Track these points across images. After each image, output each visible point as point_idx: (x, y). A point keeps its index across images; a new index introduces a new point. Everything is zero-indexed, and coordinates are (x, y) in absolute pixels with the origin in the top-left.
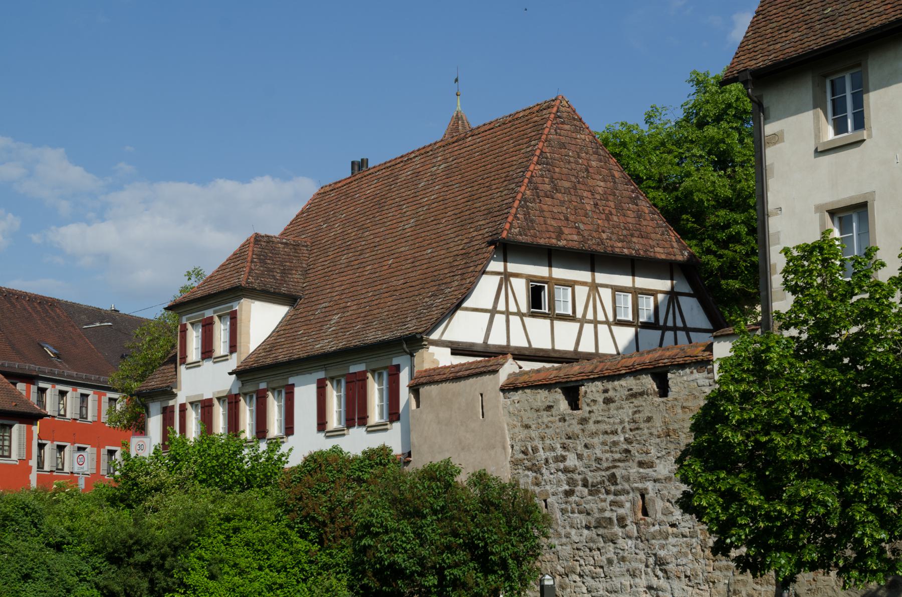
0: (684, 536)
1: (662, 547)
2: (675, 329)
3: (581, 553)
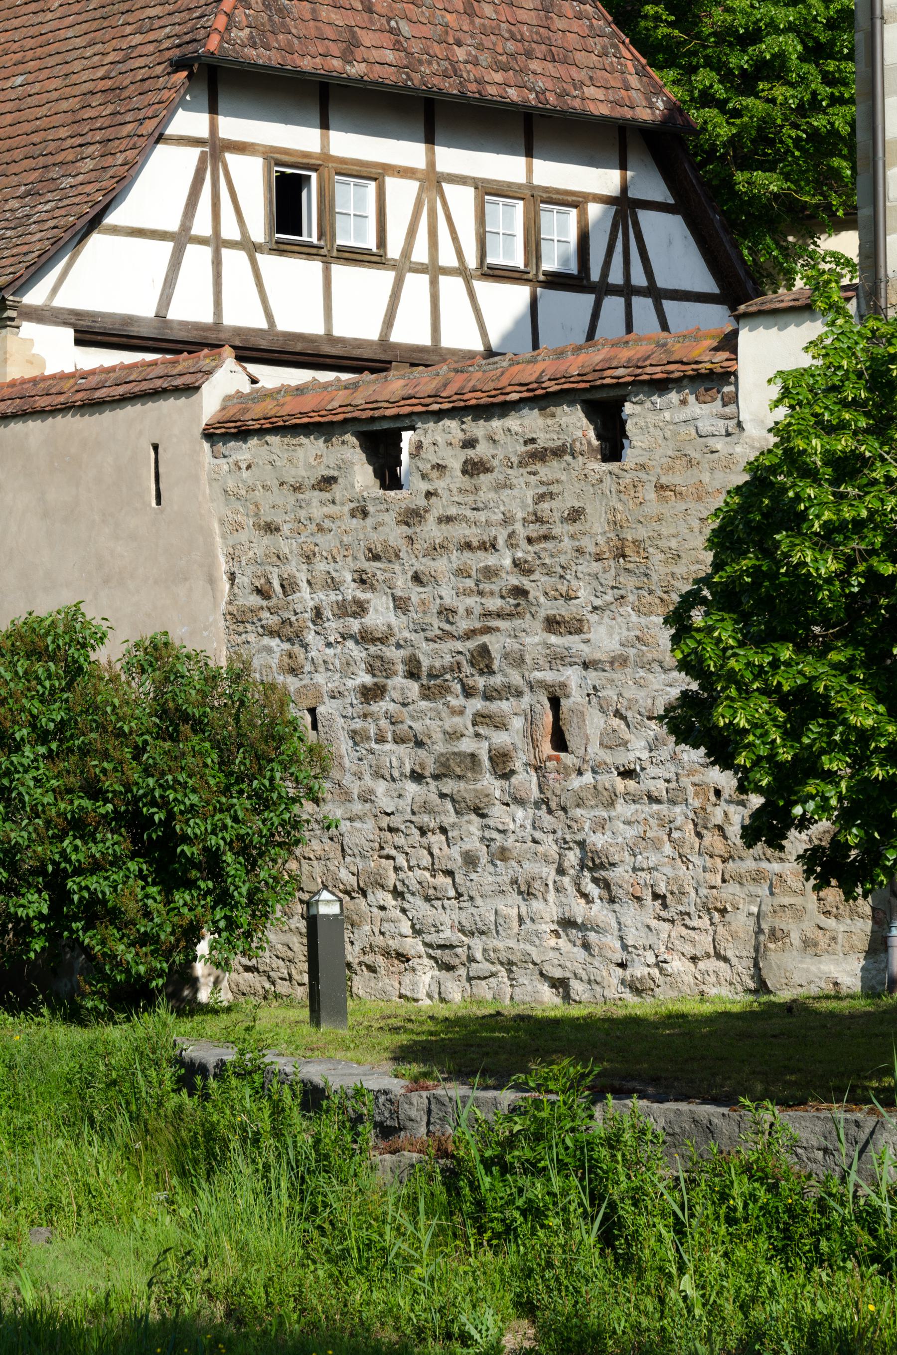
0: (653, 799)
1: (601, 825)
2: (627, 291)
3: (400, 840)
